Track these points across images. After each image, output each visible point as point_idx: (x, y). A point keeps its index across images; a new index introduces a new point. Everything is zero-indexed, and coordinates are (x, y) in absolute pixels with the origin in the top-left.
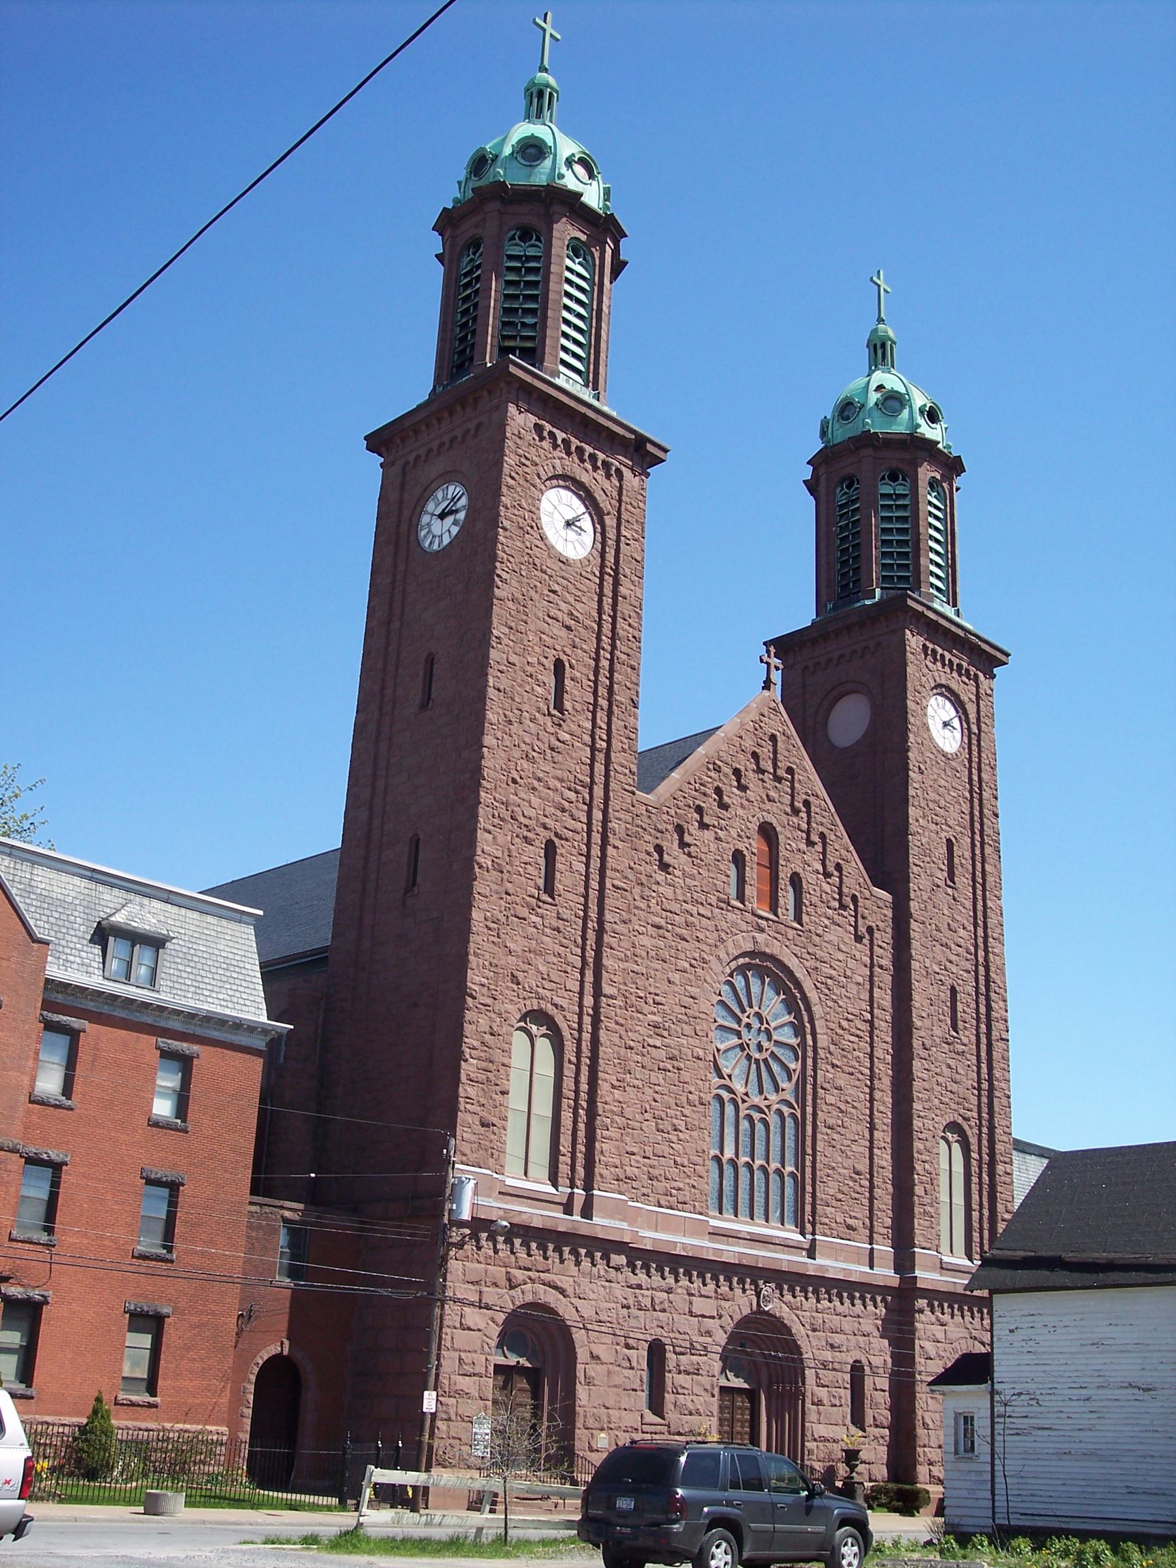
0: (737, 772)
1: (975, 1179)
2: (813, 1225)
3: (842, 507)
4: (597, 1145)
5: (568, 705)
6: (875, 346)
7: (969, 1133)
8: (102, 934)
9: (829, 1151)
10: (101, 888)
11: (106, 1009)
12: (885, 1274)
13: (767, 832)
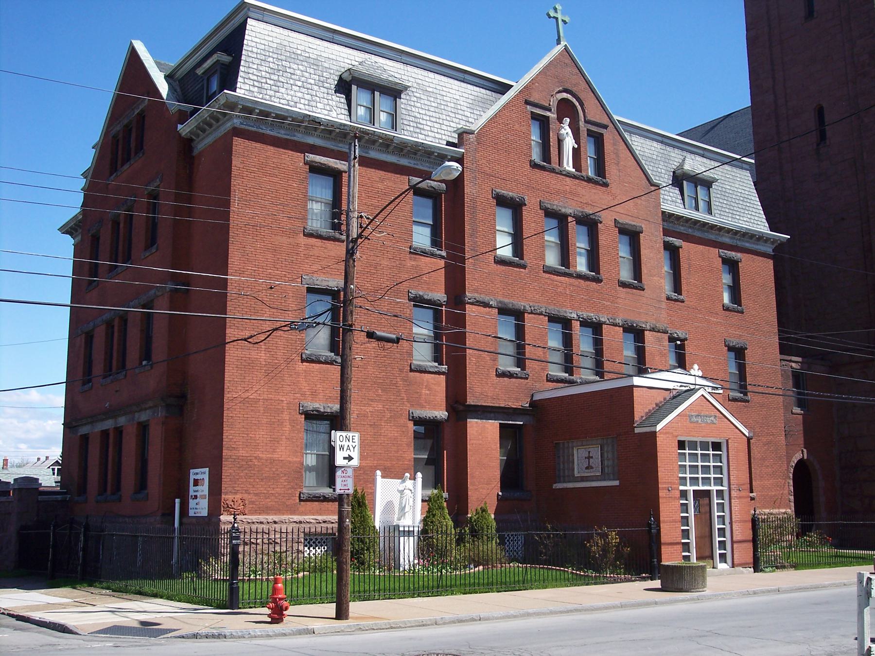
8: (345, 86)
10: (668, 149)
11: (698, 234)
12: (336, 282)
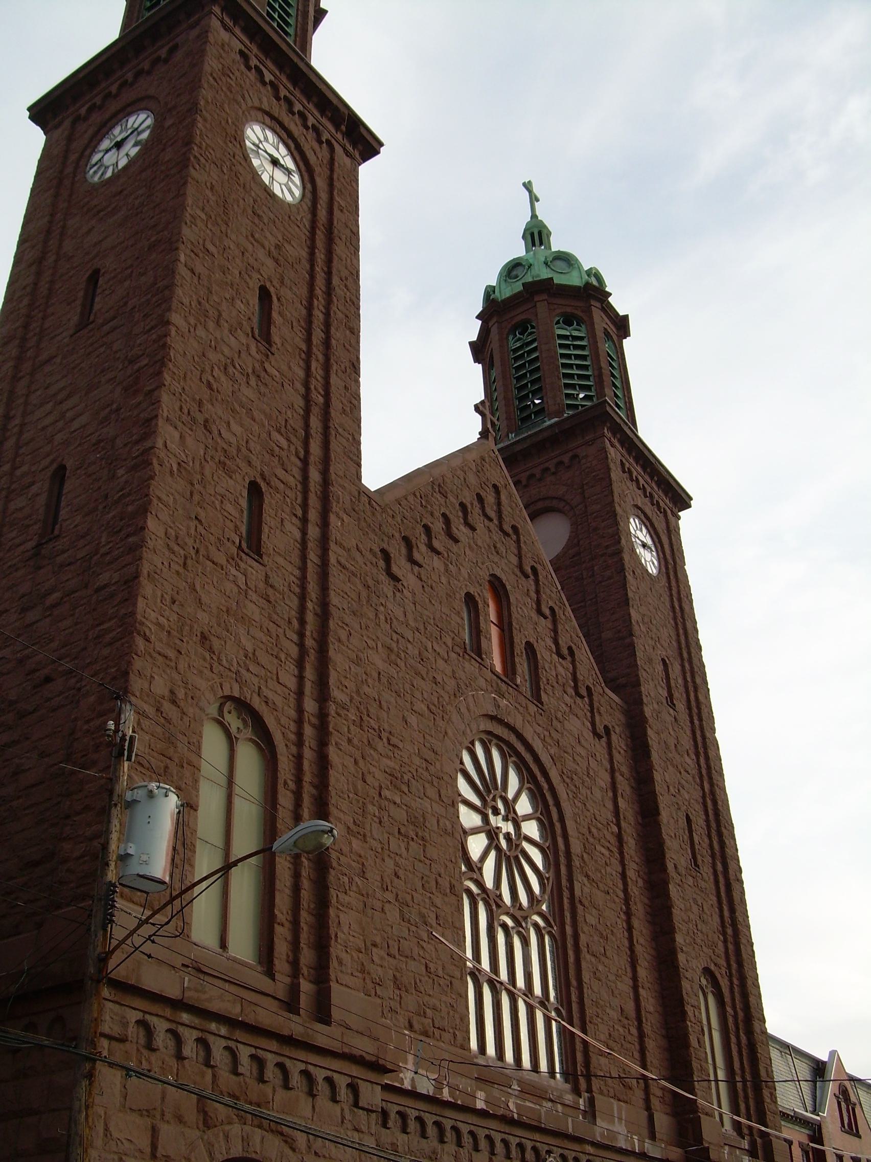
0: (463, 506)
1: (733, 1039)
2: (588, 1077)
3: (515, 351)
4: (332, 912)
5: (276, 338)
6: (532, 235)
7: (722, 983)
9: (596, 985)
13: (498, 588)
